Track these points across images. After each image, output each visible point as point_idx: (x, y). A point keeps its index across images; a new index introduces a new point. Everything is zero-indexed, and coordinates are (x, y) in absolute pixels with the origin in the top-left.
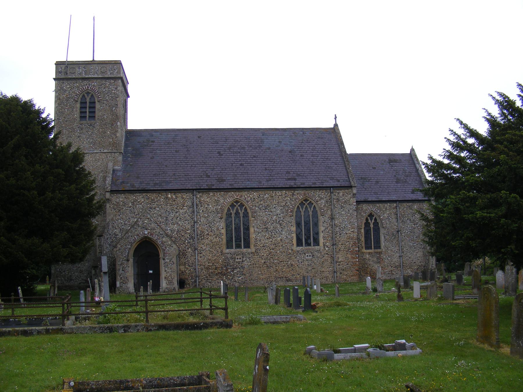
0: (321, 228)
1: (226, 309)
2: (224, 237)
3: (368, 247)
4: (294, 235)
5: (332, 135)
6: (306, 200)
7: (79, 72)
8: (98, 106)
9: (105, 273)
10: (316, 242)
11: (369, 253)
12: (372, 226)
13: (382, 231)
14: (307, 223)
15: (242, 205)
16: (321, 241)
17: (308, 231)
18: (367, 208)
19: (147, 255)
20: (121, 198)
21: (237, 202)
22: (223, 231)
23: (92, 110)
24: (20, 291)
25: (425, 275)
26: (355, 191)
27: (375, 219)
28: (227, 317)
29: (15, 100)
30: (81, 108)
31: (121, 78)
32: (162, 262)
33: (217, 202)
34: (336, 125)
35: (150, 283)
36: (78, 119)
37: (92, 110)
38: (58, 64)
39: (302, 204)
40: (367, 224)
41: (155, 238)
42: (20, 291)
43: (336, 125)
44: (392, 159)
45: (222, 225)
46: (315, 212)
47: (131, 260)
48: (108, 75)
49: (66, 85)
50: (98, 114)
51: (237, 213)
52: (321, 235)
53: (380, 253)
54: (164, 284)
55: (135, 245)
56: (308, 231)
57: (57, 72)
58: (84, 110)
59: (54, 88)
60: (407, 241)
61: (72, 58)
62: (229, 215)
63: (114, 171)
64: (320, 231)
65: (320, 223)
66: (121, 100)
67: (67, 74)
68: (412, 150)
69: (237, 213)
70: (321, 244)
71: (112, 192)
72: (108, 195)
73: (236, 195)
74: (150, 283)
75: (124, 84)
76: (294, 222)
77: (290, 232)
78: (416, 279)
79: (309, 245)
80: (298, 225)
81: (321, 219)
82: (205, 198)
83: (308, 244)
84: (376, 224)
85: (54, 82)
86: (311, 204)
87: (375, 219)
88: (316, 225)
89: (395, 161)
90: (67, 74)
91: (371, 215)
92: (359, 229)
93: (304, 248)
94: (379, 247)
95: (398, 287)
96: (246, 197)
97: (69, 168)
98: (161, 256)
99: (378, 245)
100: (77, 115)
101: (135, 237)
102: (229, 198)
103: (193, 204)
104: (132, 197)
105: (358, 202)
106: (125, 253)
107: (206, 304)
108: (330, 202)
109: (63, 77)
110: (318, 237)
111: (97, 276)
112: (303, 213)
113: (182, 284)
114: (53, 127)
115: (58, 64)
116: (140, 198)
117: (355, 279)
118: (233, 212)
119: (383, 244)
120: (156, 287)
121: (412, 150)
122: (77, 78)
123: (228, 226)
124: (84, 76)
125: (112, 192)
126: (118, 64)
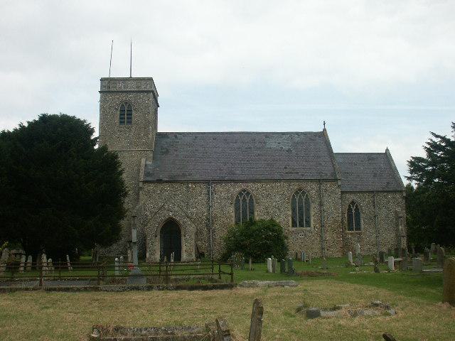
0: (312, 213)
1: (231, 274)
2: (233, 219)
3: (351, 229)
4: (290, 219)
5: (323, 135)
6: (300, 190)
7: (121, 86)
8: (133, 113)
9: (135, 243)
10: (308, 224)
11: (351, 234)
12: (353, 211)
13: (362, 215)
14: (301, 208)
15: (248, 193)
16: (312, 223)
17: (301, 215)
18: (352, 197)
19: (171, 232)
20: (152, 187)
21: (244, 191)
22: (233, 214)
23: (129, 116)
24: (68, 258)
25: (397, 252)
26: (339, 183)
27: (357, 207)
28: (232, 281)
29: (44, 119)
30: (121, 115)
31: (153, 92)
32: (183, 238)
33: (228, 191)
34: (325, 130)
35: (172, 255)
36: (118, 124)
37: (129, 116)
38: (102, 80)
39: (297, 193)
40: (350, 210)
41: (178, 219)
42: (68, 258)
43: (325, 130)
44: (370, 157)
45: (232, 209)
46: (307, 200)
47: (159, 237)
48: (143, 88)
49: (109, 97)
50: (134, 120)
51: (244, 200)
52: (312, 219)
53: (360, 234)
54: (184, 256)
55: (162, 225)
56: (301, 215)
57: (102, 86)
58: (123, 116)
59: (99, 99)
60: (385, 225)
61: (115, 74)
62: (237, 200)
63: (146, 165)
64: (312, 215)
65: (312, 209)
66: (151, 110)
67: (110, 87)
68: (387, 150)
69: (244, 200)
70: (312, 226)
71: (145, 182)
72: (141, 185)
73: (243, 186)
74: (172, 255)
75: (155, 96)
76: (290, 207)
77: (287, 216)
78: (390, 254)
79: (302, 226)
80: (294, 210)
81: (313, 205)
82: (219, 188)
83: (301, 225)
84: (357, 209)
85: (99, 95)
86: (304, 193)
87: (357, 207)
88: (308, 210)
89: (373, 159)
90: (110, 87)
91: (353, 203)
92: (343, 213)
93: (298, 228)
94: (360, 229)
95: (376, 262)
96: (251, 187)
97: (108, 164)
98: (182, 233)
99: (358, 228)
100: (117, 120)
101: (163, 217)
102: (236, 189)
103: (209, 191)
104: (160, 186)
105: (342, 193)
106: (153, 228)
107: (216, 269)
108: (319, 191)
109: (107, 90)
110: (310, 220)
111: (130, 248)
112: (297, 201)
113: (200, 255)
114: (96, 139)
115: (102, 80)
116: (167, 187)
117: (340, 255)
118: (241, 199)
119: (362, 226)
120: (178, 258)
121: (387, 150)
122: (118, 92)
123: (237, 209)
124: (123, 89)
125: (145, 182)
126: (151, 79)
